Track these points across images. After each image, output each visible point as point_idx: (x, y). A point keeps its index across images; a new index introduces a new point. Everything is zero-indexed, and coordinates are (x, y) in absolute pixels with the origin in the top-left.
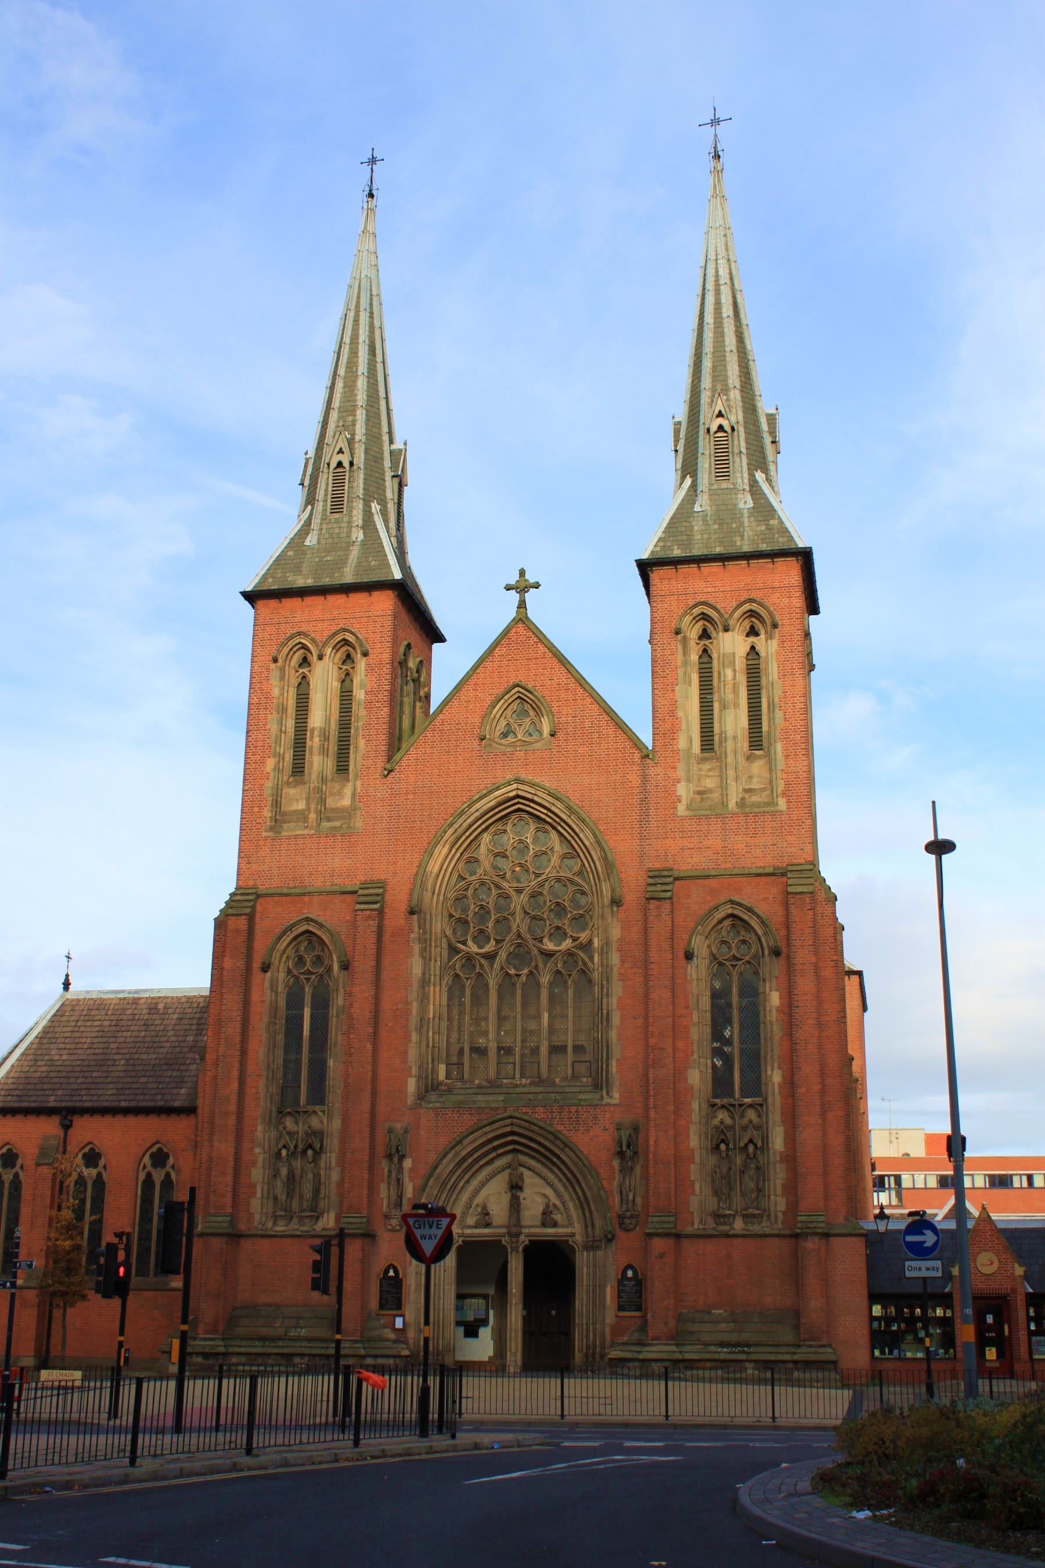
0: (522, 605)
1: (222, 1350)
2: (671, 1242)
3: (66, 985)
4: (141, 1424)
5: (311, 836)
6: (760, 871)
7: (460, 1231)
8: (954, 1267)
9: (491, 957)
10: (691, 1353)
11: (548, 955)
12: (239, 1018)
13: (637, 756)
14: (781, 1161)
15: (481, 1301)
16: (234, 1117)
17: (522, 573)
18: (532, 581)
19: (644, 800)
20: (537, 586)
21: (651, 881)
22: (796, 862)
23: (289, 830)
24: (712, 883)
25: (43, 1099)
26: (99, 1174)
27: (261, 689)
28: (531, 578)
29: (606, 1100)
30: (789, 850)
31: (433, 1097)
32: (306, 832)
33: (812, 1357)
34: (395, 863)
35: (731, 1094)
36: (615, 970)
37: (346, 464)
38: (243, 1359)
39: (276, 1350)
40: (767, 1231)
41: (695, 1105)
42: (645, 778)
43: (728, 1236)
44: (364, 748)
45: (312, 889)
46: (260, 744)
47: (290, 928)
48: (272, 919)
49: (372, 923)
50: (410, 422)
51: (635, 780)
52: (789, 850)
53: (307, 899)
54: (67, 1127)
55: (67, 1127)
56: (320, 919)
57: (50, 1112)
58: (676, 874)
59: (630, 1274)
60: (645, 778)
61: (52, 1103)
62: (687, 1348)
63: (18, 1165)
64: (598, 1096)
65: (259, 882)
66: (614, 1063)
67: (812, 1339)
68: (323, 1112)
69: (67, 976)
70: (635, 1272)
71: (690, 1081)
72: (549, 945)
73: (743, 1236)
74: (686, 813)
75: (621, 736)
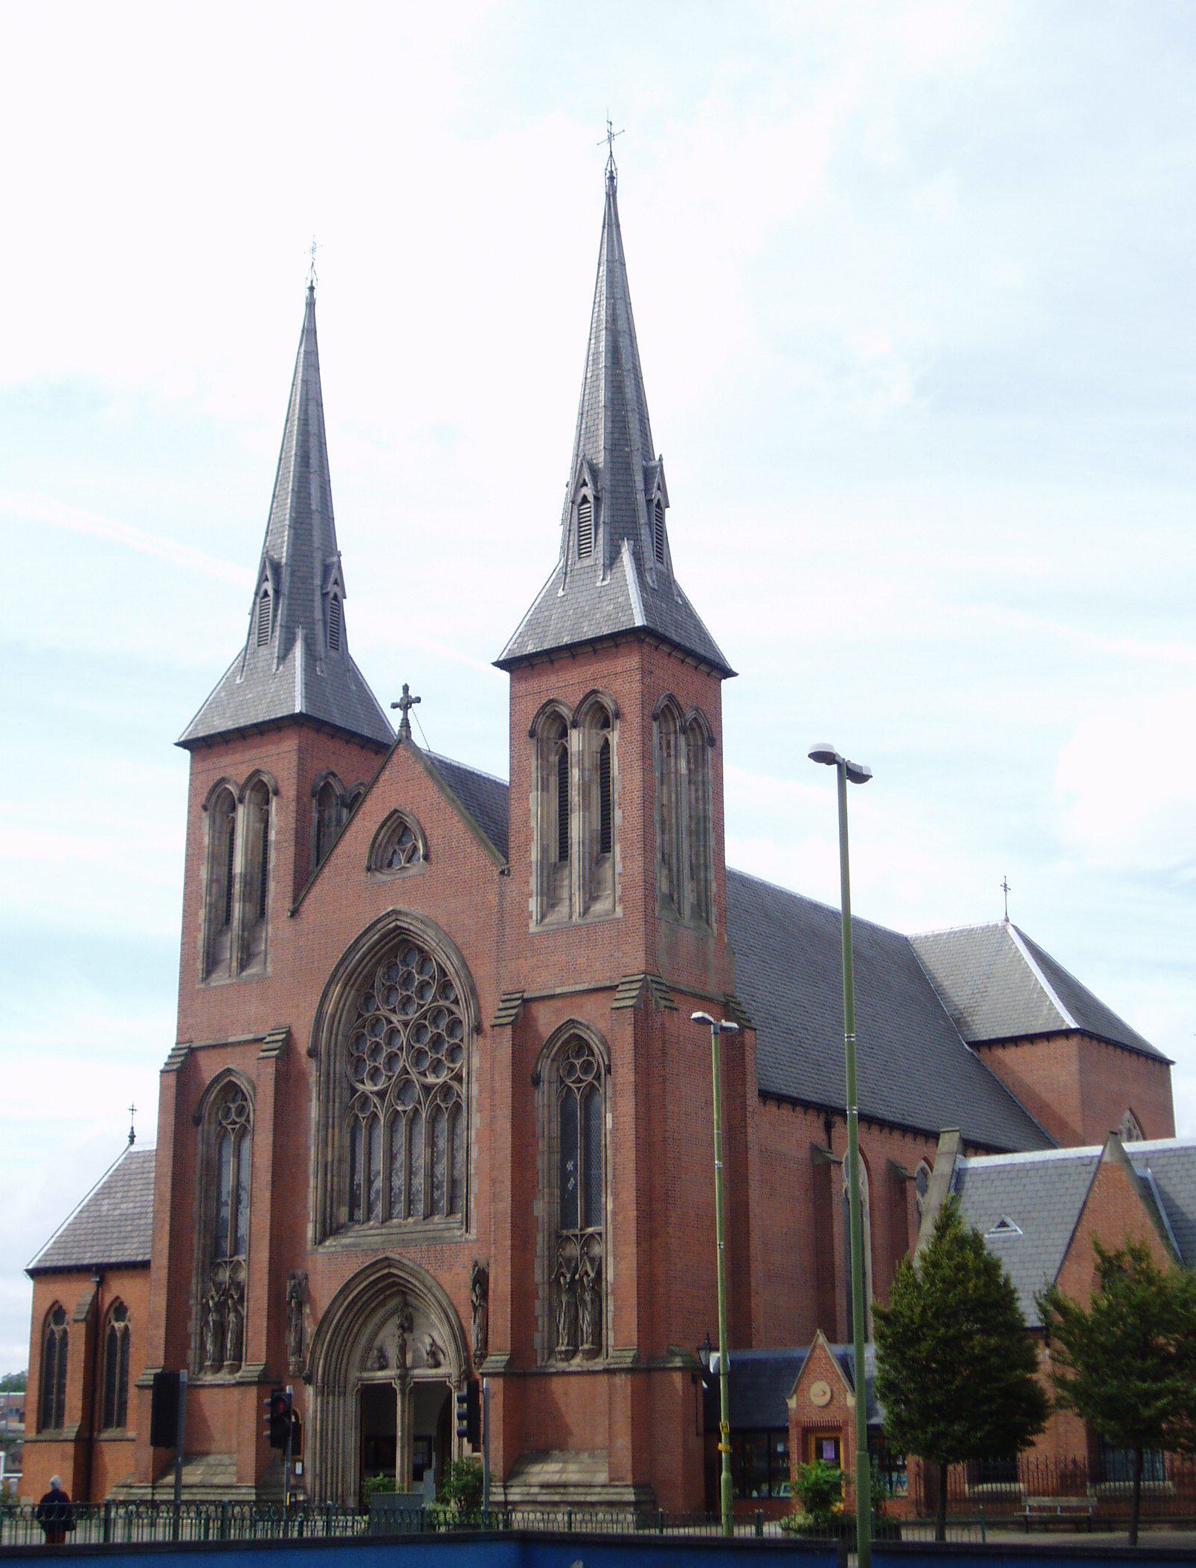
3: (132, 1137)
7: (358, 1374)
8: (790, 1398)
11: (427, 1089)
13: (496, 873)
15: (425, 1444)
17: (406, 688)
20: (418, 700)
21: (501, 1005)
22: (630, 972)
26: (126, 1328)
28: (412, 694)
30: (625, 960)
33: (615, 1498)
37: (591, 499)
41: (540, 1238)
42: (502, 895)
44: (279, 891)
48: (210, 1068)
50: (668, 438)
51: (493, 899)
52: (625, 960)
58: (526, 995)
60: (502, 895)
71: (536, 1214)
72: (431, 1079)
74: (539, 929)
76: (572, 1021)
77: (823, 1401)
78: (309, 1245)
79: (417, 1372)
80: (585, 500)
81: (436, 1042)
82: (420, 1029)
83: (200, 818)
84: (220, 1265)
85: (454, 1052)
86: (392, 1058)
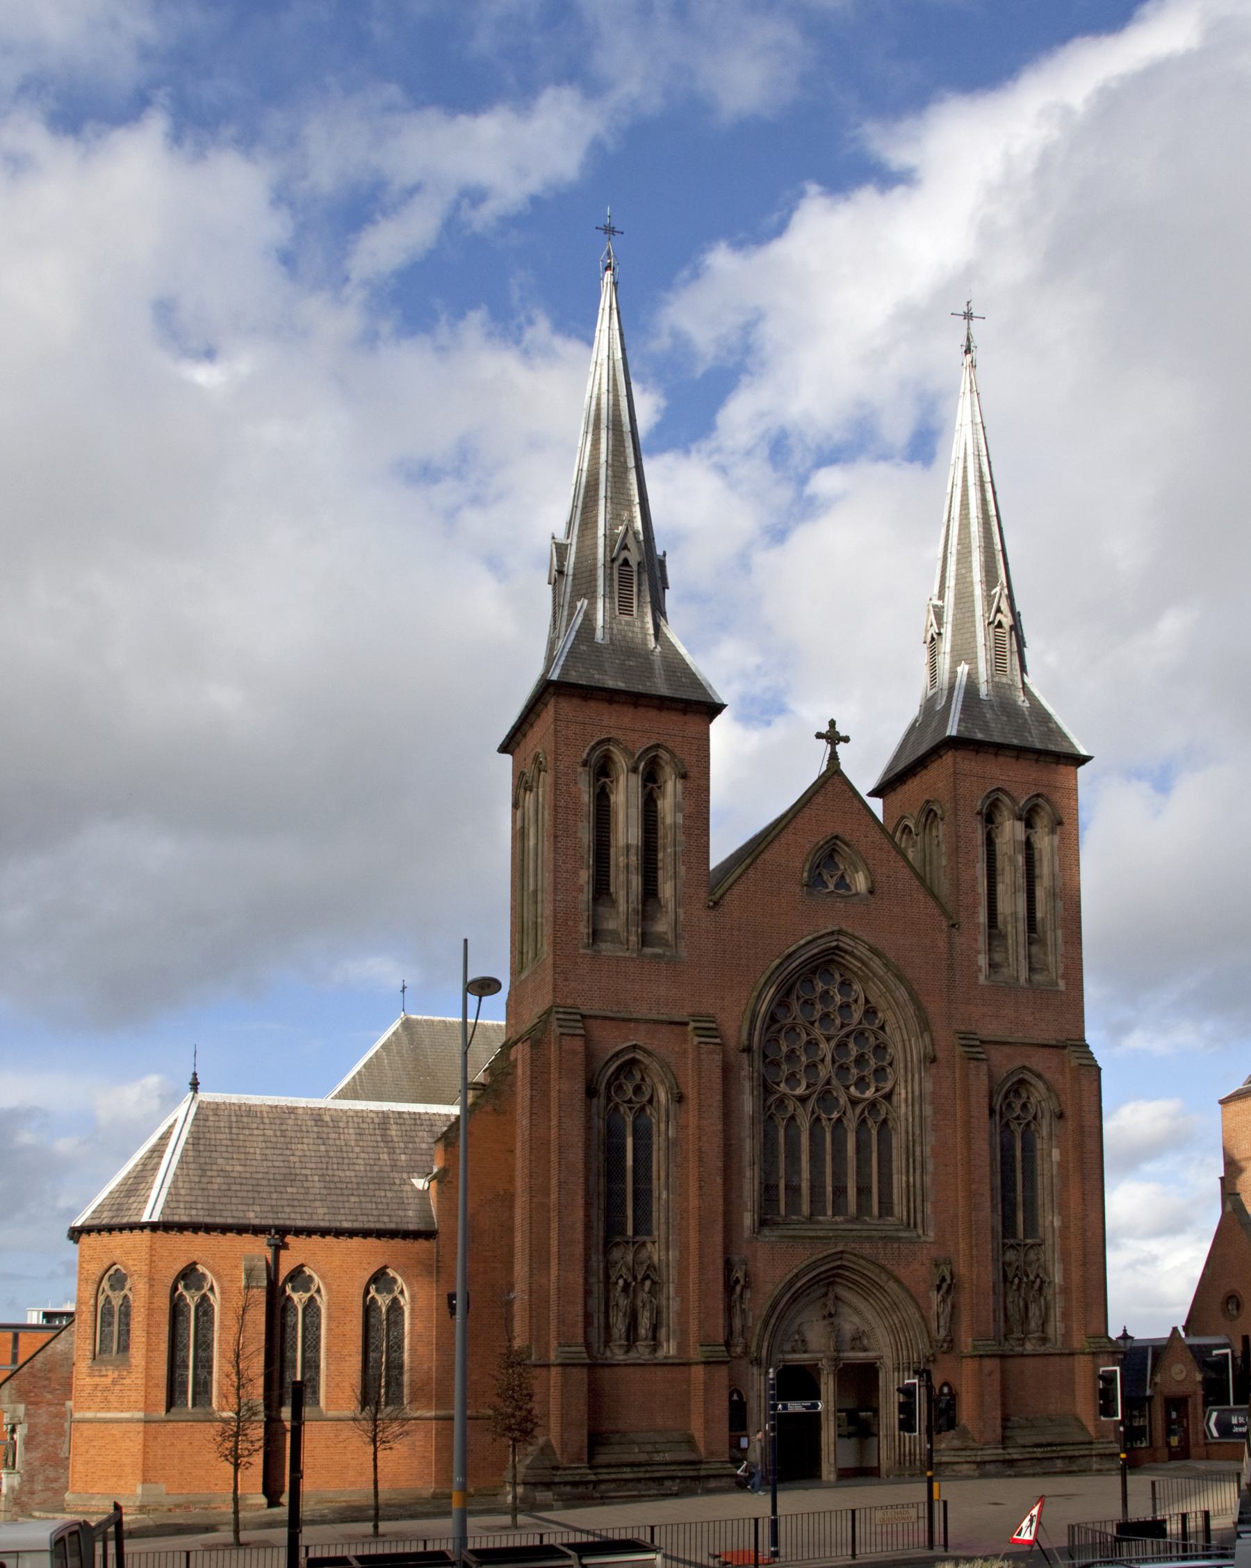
0: (834, 757)
1: (593, 1478)
2: (997, 1361)
4: (760, 1558)
5: (633, 959)
6: (1046, 1042)
7: (781, 1356)
9: (803, 1100)
10: (1015, 1454)
11: (854, 1102)
12: (580, 1144)
13: (945, 925)
14: (1060, 1293)
16: (581, 1246)
18: (827, 728)
19: (951, 967)
23: (606, 948)
24: (1006, 1049)
25: (241, 1214)
26: (312, 1299)
27: (568, 792)
28: (842, 730)
29: (923, 1239)
31: (766, 1231)
32: (627, 954)
34: (723, 999)
35: (1014, 1236)
36: (929, 1120)
38: (613, 1486)
39: (648, 1475)
40: (1052, 1351)
42: (951, 945)
43: (1022, 1355)
45: (639, 1016)
46: (571, 852)
47: (617, 1055)
49: (717, 1057)
53: (632, 1025)
54: (278, 1248)
55: (278, 1248)
56: (649, 1047)
57: (257, 1230)
59: (946, 1390)
60: (951, 945)
61: (253, 1218)
62: (1010, 1451)
63: (128, 1287)
64: (914, 1234)
65: (579, 1002)
66: (929, 1208)
67: (1103, 1437)
68: (654, 1243)
69: (195, 1074)
70: (950, 1389)
73: (1034, 1355)
75: (931, 903)
76: (1024, 1067)
77: (1179, 1378)
78: (747, 1234)
79: (846, 1354)
80: (1000, 625)
81: (860, 1060)
82: (842, 1045)
83: (575, 771)
84: (617, 1244)
85: (880, 1073)
86: (812, 1066)
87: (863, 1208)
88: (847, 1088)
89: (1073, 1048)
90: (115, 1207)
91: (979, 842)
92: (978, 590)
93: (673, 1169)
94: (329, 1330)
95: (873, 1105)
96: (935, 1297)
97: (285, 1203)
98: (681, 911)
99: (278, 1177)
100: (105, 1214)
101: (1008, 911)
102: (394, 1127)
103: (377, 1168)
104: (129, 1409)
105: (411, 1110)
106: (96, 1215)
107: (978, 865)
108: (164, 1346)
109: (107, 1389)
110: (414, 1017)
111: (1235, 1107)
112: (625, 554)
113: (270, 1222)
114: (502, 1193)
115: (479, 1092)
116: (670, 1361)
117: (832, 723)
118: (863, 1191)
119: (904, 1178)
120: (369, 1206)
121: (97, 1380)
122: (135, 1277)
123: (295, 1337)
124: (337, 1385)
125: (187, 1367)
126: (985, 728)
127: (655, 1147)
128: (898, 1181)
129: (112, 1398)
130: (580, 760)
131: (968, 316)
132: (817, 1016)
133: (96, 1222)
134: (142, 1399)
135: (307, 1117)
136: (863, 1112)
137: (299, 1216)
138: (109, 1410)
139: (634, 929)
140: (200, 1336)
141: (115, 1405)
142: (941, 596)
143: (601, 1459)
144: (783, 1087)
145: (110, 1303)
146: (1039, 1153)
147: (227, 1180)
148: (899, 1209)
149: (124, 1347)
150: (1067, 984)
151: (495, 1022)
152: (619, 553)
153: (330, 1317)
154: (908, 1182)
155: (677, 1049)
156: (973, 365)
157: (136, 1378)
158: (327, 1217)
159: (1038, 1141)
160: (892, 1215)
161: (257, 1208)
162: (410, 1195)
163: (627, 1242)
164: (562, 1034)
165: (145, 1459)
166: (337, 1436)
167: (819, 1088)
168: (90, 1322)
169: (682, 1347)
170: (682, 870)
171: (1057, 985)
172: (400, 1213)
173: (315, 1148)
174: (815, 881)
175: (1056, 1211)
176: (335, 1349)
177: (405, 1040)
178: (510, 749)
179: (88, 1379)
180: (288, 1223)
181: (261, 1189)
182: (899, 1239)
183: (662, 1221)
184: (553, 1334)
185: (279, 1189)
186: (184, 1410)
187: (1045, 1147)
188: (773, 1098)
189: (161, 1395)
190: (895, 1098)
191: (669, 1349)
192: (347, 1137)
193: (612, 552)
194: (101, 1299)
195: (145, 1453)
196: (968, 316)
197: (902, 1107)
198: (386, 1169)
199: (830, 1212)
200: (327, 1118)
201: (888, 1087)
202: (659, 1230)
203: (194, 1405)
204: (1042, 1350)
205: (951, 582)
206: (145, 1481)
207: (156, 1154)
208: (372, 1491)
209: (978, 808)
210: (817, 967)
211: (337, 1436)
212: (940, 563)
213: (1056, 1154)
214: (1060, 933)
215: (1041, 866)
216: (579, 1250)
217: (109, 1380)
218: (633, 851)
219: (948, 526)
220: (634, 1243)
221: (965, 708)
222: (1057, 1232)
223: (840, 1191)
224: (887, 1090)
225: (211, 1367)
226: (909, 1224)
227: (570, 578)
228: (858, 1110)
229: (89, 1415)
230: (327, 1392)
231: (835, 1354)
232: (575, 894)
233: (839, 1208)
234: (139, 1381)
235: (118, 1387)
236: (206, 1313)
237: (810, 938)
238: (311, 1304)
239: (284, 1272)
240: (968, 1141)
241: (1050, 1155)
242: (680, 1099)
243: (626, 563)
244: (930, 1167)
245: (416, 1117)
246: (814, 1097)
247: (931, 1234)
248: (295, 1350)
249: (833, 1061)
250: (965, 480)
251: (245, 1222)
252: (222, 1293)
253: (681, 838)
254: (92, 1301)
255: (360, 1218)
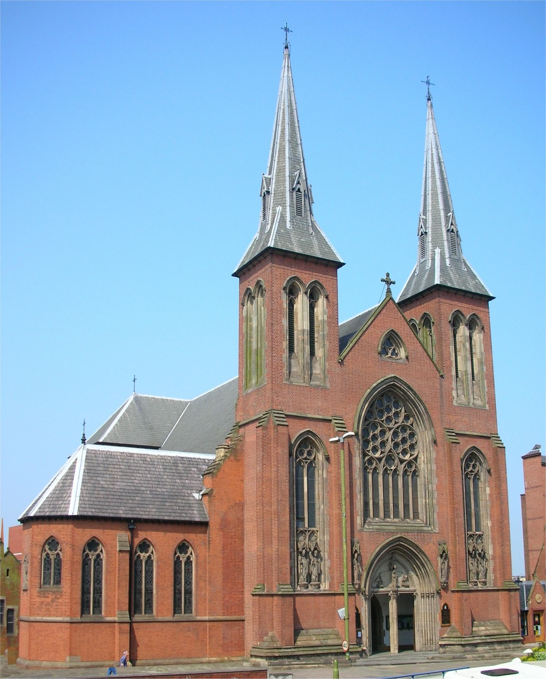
0: (389, 291)
9: (380, 459)
13: (438, 375)
14: (492, 559)
19: (441, 397)
26: (149, 557)
32: (304, 385)
34: (346, 408)
42: (441, 385)
60: (441, 385)
63: (59, 549)
64: (430, 529)
65: (283, 408)
66: (436, 517)
69: (84, 435)
85: (412, 447)
87: (406, 515)
88: (398, 454)
89: (494, 438)
90: (51, 506)
91: (451, 336)
92: (442, 213)
93: (325, 494)
94: (158, 573)
95: (410, 464)
96: (440, 560)
97: (136, 505)
98: (327, 364)
99: (130, 491)
100: (46, 510)
101: (300, 328)
102: (180, 465)
103: (176, 487)
104: (61, 616)
105: (187, 456)
106: (41, 510)
107: (451, 347)
108: (80, 582)
109: (48, 604)
110: (139, 395)
111: (528, 460)
112: (298, 186)
113: (130, 516)
114: (238, 502)
115: (227, 450)
116: (326, 592)
117: (388, 275)
118: (406, 506)
119: (424, 500)
120: (175, 507)
121: (43, 599)
122: (64, 544)
123: (141, 577)
124: (162, 603)
125: (90, 593)
126: (451, 281)
127: (317, 482)
128: (421, 502)
129: (51, 609)
130: (282, 287)
131: (428, 83)
132: (384, 418)
133: (42, 514)
134: (69, 610)
135: (139, 459)
136: (405, 467)
137: (143, 513)
138: (50, 616)
139: (307, 372)
140: (96, 576)
141: (53, 613)
142: (425, 213)
143: (299, 643)
144: (371, 454)
145: (49, 557)
146: (480, 489)
147: (107, 493)
148: (422, 515)
149: (58, 582)
150: (489, 406)
151: (179, 400)
152: (296, 186)
153: (158, 567)
154: (426, 502)
155: (327, 433)
156: (432, 106)
157: (65, 599)
158: (157, 514)
159: (480, 483)
160: (418, 518)
161: (123, 508)
162: (194, 502)
163: (306, 531)
164: (278, 425)
165: (71, 642)
166: (162, 630)
167: (386, 454)
168: (38, 568)
169: (331, 585)
170: (327, 343)
171: (485, 407)
172: (191, 512)
173: (145, 475)
174: (384, 351)
175: (489, 519)
176: (161, 584)
177: (137, 408)
178: (239, 275)
179: (37, 599)
180: (139, 516)
181: (123, 498)
182: (423, 531)
183: (321, 520)
184: (274, 578)
185: (132, 498)
186: (88, 615)
187: (483, 486)
188: (367, 458)
189: (78, 608)
190: (418, 460)
191: (325, 587)
192: (159, 470)
193: (293, 184)
194: (44, 554)
195: (71, 639)
196: (428, 83)
197: (422, 465)
198: (180, 488)
199: (392, 517)
200: (149, 460)
201: (416, 453)
202: (319, 526)
203: (94, 613)
204: (485, 588)
205: (429, 208)
206: (71, 655)
207: (69, 478)
208: (27, 623)
209: (450, 319)
210: (384, 394)
211: (162, 630)
212: (423, 198)
213: (488, 489)
214: (485, 381)
215: (475, 348)
216: (287, 535)
217: (50, 600)
218: (306, 333)
219: (426, 181)
220: (309, 531)
221: (441, 270)
222: (490, 528)
223: (396, 506)
224: (415, 456)
225: (101, 593)
226: (426, 524)
227: (273, 195)
228: (403, 465)
229: (38, 618)
230: (157, 607)
231: (396, 589)
232: (281, 353)
233: (396, 515)
234: (66, 601)
235: (55, 604)
236: (98, 564)
237: (383, 379)
238: (149, 561)
239: (137, 541)
240: (452, 483)
241: (485, 490)
242: (328, 459)
243: (299, 190)
244: (436, 495)
245: (190, 460)
246: (384, 458)
247: (437, 529)
248: (141, 584)
249: (392, 440)
250: (432, 160)
251: (118, 516)
252: (107, 554)
253: (326, 328)
254: (39, 557)
255: (173, 514)
